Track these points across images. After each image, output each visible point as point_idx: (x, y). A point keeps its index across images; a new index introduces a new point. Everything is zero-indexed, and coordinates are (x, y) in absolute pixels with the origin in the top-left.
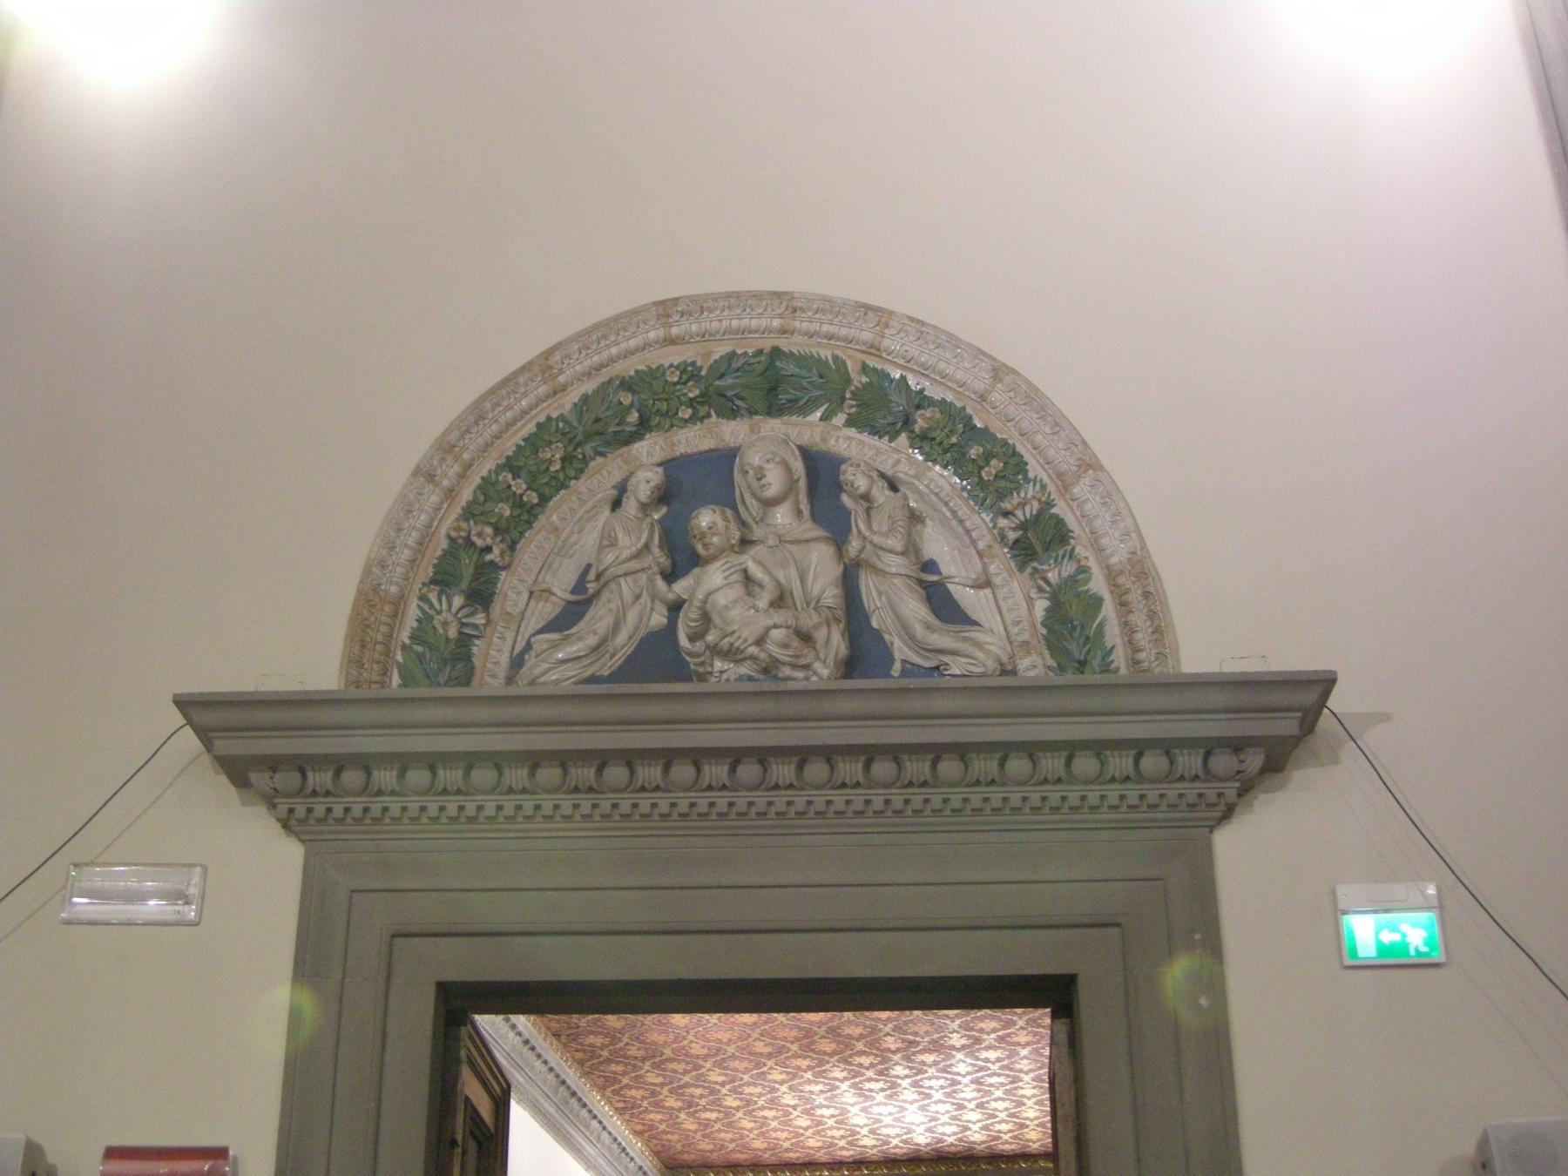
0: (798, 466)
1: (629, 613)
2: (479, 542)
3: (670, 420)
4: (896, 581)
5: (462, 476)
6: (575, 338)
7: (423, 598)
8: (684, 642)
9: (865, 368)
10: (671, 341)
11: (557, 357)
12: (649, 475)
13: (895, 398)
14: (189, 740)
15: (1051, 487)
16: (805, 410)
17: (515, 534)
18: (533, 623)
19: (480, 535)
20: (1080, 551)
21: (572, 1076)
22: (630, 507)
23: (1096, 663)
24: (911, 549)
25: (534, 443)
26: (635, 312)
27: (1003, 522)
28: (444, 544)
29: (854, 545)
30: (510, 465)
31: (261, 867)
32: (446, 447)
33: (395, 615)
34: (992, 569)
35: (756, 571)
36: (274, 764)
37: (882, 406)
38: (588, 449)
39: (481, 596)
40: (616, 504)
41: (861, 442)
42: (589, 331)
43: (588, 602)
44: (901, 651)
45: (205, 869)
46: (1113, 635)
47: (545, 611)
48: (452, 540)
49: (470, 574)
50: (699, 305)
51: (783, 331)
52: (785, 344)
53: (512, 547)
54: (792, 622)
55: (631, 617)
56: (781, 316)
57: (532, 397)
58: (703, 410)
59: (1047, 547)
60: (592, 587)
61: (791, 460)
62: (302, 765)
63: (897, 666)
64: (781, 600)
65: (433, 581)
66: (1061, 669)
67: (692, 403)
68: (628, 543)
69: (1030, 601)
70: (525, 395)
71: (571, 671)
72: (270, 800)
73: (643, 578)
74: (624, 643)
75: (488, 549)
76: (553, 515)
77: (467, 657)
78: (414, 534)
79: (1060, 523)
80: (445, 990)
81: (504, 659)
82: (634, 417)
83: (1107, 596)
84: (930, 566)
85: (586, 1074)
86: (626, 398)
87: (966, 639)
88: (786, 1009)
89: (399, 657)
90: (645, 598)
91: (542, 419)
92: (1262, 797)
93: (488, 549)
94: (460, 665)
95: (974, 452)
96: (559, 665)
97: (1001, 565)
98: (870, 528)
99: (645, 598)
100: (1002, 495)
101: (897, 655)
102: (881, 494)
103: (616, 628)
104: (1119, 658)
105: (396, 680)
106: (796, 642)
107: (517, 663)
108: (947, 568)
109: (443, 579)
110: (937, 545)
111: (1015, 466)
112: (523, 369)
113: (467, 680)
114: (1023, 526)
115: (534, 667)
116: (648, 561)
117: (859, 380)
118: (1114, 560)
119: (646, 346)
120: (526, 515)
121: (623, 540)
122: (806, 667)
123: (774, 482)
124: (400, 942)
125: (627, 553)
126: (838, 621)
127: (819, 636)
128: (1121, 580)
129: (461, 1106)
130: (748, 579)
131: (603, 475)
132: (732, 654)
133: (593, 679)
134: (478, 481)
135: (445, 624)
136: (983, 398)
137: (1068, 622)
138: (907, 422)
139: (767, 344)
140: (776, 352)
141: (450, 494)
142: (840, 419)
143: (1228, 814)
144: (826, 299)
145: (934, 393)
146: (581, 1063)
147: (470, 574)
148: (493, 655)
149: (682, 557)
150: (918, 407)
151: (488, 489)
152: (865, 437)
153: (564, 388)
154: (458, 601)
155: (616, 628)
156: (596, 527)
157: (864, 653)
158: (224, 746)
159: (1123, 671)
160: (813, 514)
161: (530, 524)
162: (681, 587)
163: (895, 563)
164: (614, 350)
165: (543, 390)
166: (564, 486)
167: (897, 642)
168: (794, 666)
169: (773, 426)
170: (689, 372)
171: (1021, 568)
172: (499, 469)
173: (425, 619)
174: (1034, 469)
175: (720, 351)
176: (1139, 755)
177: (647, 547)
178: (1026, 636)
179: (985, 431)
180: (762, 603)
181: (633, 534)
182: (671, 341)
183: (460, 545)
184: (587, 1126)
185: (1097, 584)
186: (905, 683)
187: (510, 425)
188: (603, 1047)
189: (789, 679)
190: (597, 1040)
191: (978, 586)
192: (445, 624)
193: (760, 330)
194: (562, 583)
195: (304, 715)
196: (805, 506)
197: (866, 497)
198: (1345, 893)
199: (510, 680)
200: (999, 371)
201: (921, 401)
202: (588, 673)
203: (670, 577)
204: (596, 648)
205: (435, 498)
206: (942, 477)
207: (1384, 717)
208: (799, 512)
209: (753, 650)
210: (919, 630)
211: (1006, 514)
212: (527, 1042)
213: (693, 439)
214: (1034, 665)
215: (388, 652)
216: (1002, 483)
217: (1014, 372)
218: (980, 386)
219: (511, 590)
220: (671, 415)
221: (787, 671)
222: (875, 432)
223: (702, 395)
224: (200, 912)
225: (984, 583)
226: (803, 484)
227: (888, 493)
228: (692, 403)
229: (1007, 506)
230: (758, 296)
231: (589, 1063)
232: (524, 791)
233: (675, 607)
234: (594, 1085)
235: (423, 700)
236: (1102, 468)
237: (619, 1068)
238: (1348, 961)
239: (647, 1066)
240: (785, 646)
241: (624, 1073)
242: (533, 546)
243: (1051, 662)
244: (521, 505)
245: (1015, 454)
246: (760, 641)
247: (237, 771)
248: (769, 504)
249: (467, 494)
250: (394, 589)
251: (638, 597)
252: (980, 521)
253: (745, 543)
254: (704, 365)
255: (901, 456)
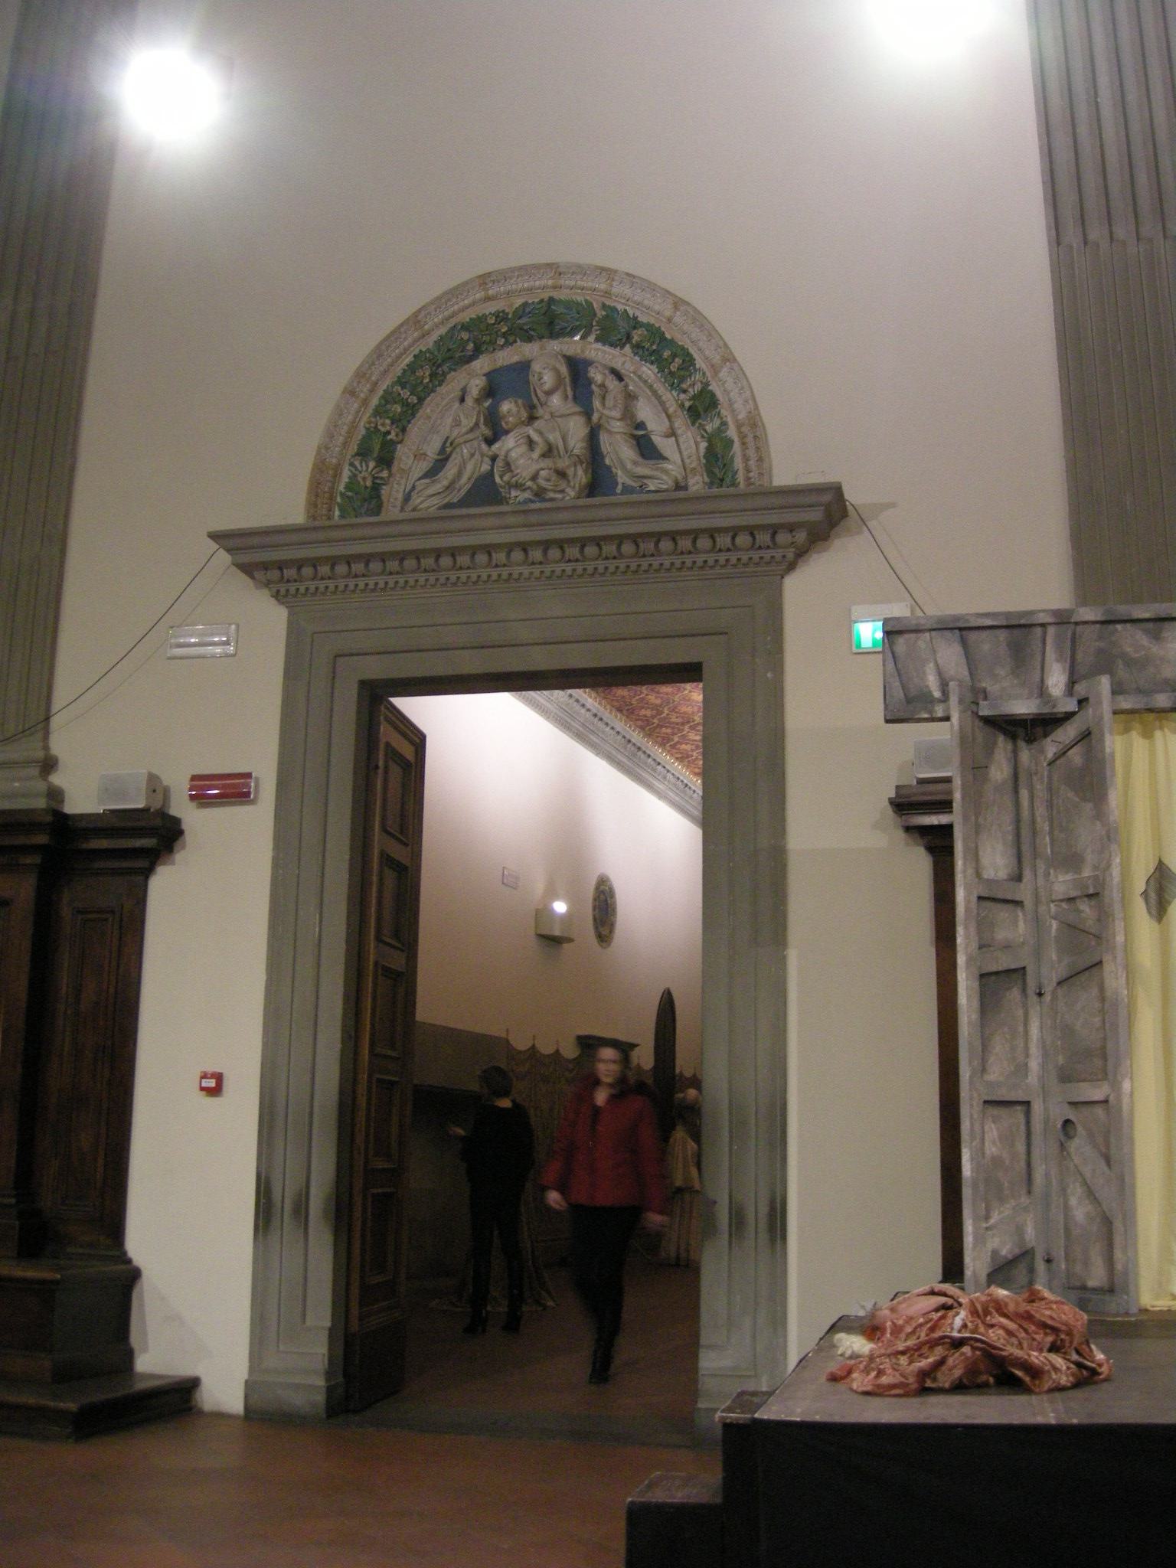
0: (564, 370)
1: (468, 465)
2: (383, 429)
3: (493, 346)
4: (618, 437)
5: (372, 391)
6: (431, 303)
7: (352, 464)
8: (498, 479)
9: (604, 306)
10: (488, 299)
11: (423, 313)
12: (478, 382)
13: (620, 323)
14: (224, 558)
15: (708, 374)
16: (572, 334)
17: (405, 422)
18: (417, 473)
19: (383, 425)
20: (724, 412)
21: (636, 737)
22: (469, 401)
23: (728, 480)
24: (628, 415)
25: (412, 368)
26: (466, 283)
27: (682, 396)
28: (363, 432)
29: (595, 417)
30: (401, 382)
31: (268, 620)
32: (360, 375)
33: (335, 476)
34: (676, 425)
35: (535, 437)
36: (265, 566)
37: (615, 328)
38: (445, 368)
39: (386, 460)
40: (462, 400)
41: (604, 352)
42: (439, 298)
43: (447, 459)
44: (622, 478)
45: (238, 626)
46: (738, 464)
47: (424, 466)
48: (368, 429)
49: (380, 451)
50: (504, 275)
51: (554, 287)
52: (555, 294)
53: (404, 430)
54: (551, 465)
55: (470, 467)
56: (552, 278)
57: (410, 340)
58: (511, 339)
59: (706, 410)
60: (448, 450)
61: (558, 366)
62: (281, 566)
63: (620, 487)
64: (549, 452)
65: (357, 454)
66: (711, 484)
67: (504, 335)
68: (467, 423)
69: (697, 443)
70: (405, 339)
71: (435, 501)
72: (267, 584)
73: (475, 443)
74: (465, 484)
75: (389, 433)
76: (427, 409)
77: (379, 497)
78: (345, 427)
79: (713, 395)
80: (363, 684)
81: (400, 496)
82: (471, 346)
83: (736, 439)
84: (641, 426)
85: (649, 735)
86: (465, 335)
87: (657, 469)
88: (562, 688)
89: (339, 500)
90: (477, 456)
91: (417, 352)
92: (815, 556)
93: (389, 433)
94: (374, 501)
95: (666, 354)
96: (429, 499)
97: (681, 423)
98: (604, 405)
99: (477, 456)
100: (682, 379)
101: (620, 480)
102: (612, 384)
103: (459, 474)
104: (741, 477)
105: (337, 513)
106: (554, 477)
107: (407, 498)
108: (650, 426)
109: (363, 453)
110: (645, 411)
111: (689, 362)
112: (402, 325)
113: (378, 510)
114: (693, 398)
115: (416, 500)
116: (477, 433)
117: (601, 313)
118: (740, 417)
119: (474, 304)
120: (411, 410)
121: (464, 421)
122: (562, 491)
123: (548, 380)
124: (341, 660)
125: (464, 430)
126: (581, 463)
127: (570, 472)
128: (743, 429)
129: (382, 746)
130: (531, 444)
131: (456, 380)
132: (518, 486)
133: (449, 506)
134: (381, 393)
135: (364, 479)
136: (669, 320)
137: (716, 458)
138: (629, 337)
139: (546, 296)
140: (551, 300)
141: (365, 402)
142: (591, 338)
143: (791, 567)
144: (579, 266)
145: (643, 319)
146: (642, 728)
147: (380, 451)
148: (393, 493)
149: (496, 432)
150: (635, 328)
151: (388, 398)
152: (607, 348)
153: (428, 333)
154: (372, 464)
155: (459, 474)
156: (447, 415)
157: (599, 480)
158: (246, 558)
159: (742, 486)
160: (575, 398)
161: (413, 415)
162: (496, 446)
163: (618, 426)
164: (456, 307)
165: (416, 335)
166: (433, 391)
167: (619, 473)
168: (555, 492)
169: (555, 345)
170: (501, 317)
171: (693, 424)
172: (394, 384)
173: (353, 477)
174: (700, 363)
175: (518, 302)
176: (774, 534)
177: (477, 424)
178: (694, 465)
179: (672, 341)
180: (536, 455)
181: (469, 416)
182: (488, 299)
183: (372, 432)
184: (655, 770)
185: (732, 432)
186: (624, 498)
187: (399, 357)
188: (653, 717)
189: (552, 500)
190: (649, 713)
191: (667, 436)
192: (364, 479)
193: (540, 288)
194: (432, 449)
195: (255, 541)
196: (570, 393)
197: (602, 386)
198: (856, 611)
199: (402, 510)
200: (678, 303)
201: (636, 324)
202: (446, 501)
203: (490, 442)
204: (448, 488)
205: (356, 405)
206: (649, 371)
207: (893, 505)
208: (566, 397)
209: (529, 484)
210: (629, 466)
211: (685, 391)
212: (595, 715)
213: (506, 357)
214: (697, 484)
215: (332, 498)
216: (682, 373)
217: (688, 304)
218: (668, 313)
219: (404, 455)
220: (493, 343)
221: (551, 495)
222: (613, 345)
223: (510, 329)
224: (236, 648)
225: (672, 433)
226: (567, 380)
227: (616, 383)
228: (504, 335)
229: (684, 386)
230: (537, 267)
231: (648, 727)
232: (398, 573)
233: (494, 459)
234: (655, 742)
235: (352, 526)
236: (735, 360)
237: (669, 731)
238: (855, 650)
239: (686, 728)
240: (548, 480)
241: (674, 734)
242: (416, 429)
243: (707, 480)
244: (408, 405)
245: (689, 354)
246: (534, 478)
247: (248, 569)
248: (549, 393)
249: (375, 401)
250: (334, 461)
251: (472, 455)
252: (669, 397)
253: (532, 419)
254: (510, 311)
255: (623, 359)
